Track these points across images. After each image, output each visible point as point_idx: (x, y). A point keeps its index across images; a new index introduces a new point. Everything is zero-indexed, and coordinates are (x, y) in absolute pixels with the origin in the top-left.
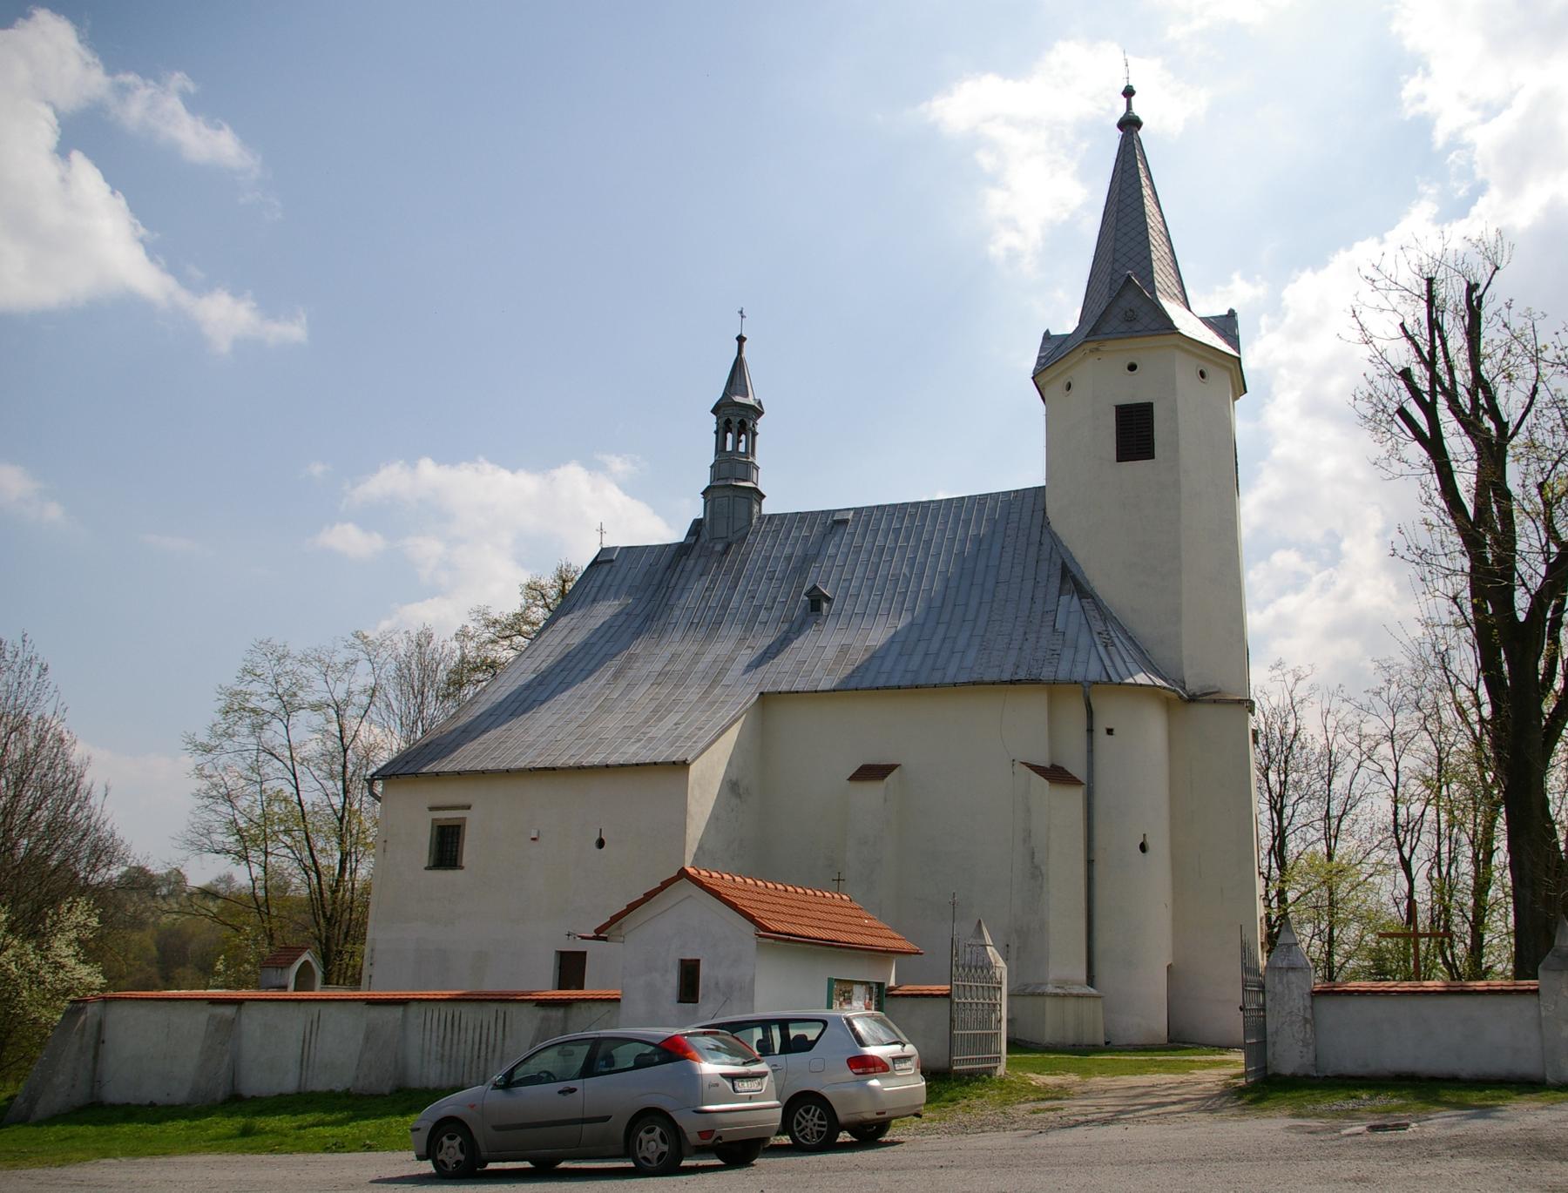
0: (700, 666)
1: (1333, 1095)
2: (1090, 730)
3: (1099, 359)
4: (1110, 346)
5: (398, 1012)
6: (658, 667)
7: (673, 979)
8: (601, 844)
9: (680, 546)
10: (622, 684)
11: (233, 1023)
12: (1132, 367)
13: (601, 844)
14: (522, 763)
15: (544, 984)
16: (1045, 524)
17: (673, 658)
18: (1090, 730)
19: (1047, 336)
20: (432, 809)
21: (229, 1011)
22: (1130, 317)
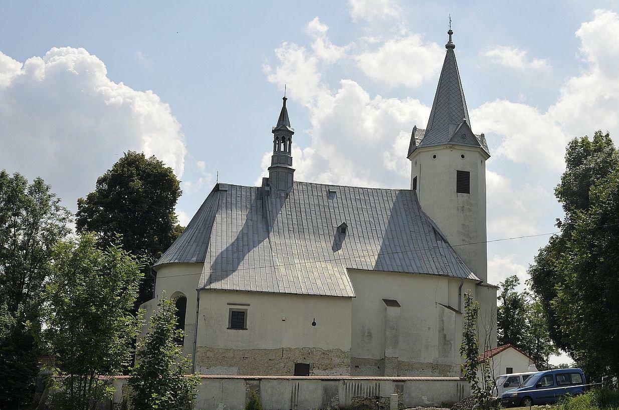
2: (460, 294)
18: (460, 294)
20: (228, 304)
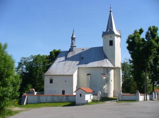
0: (72, 64)
1: (29, 110)
3: (111, 81)
4: (109, 35)
5: (54, 96)
6: (68, 64)
7: (79, 95)
8: (66, 81)
9: (68, 51)
10: (65, 66)
11: (40, 97)
12: (111, 37)
13: (66, 81)
14: (58, 74)
15: (61, 94)
16: (103, 50)
17: (69, 63)
19: (103, 32)
20: (50, 78)
21: (39, 96)
22: (111, 32)
